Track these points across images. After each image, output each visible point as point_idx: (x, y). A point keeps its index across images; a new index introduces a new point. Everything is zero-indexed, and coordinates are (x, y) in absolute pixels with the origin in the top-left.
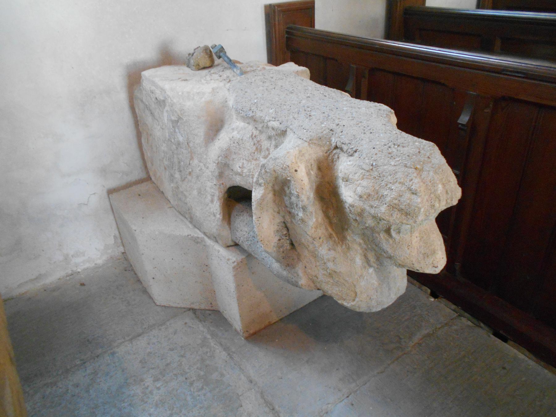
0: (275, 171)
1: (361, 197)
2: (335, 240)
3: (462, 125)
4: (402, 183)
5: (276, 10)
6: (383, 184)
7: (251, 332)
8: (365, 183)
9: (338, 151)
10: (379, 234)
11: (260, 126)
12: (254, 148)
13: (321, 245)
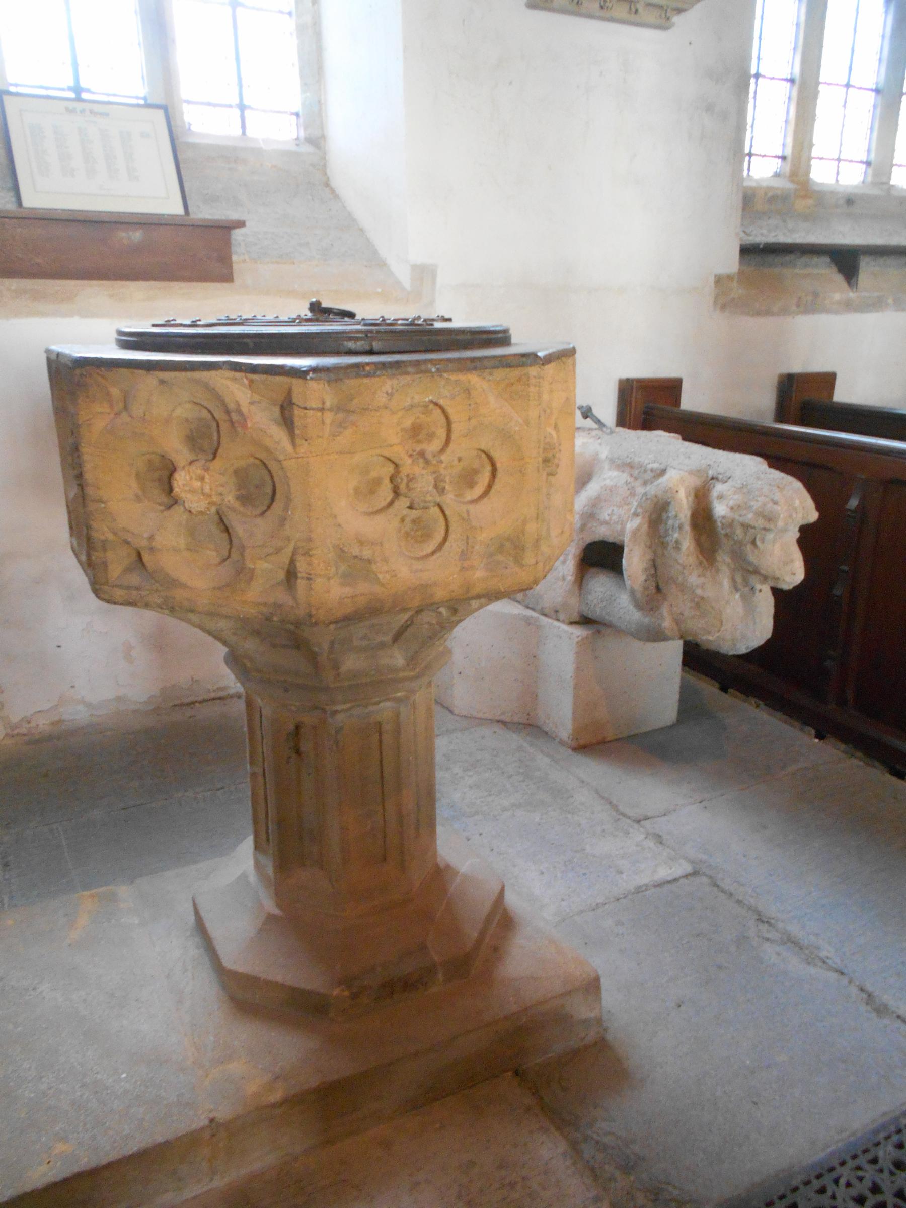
0: (656, 496)
1: (732, 508)
2: (705, 566)
3: (850, 510)
4: (766, 496)
5: (635, 386)
6: (751, 497)
7: (582, 742)
8: (736, 497)
9: (714, 481)
10: (746, 545)
11: (636, 473)
12: (628, 492)
13: (690, 574)
